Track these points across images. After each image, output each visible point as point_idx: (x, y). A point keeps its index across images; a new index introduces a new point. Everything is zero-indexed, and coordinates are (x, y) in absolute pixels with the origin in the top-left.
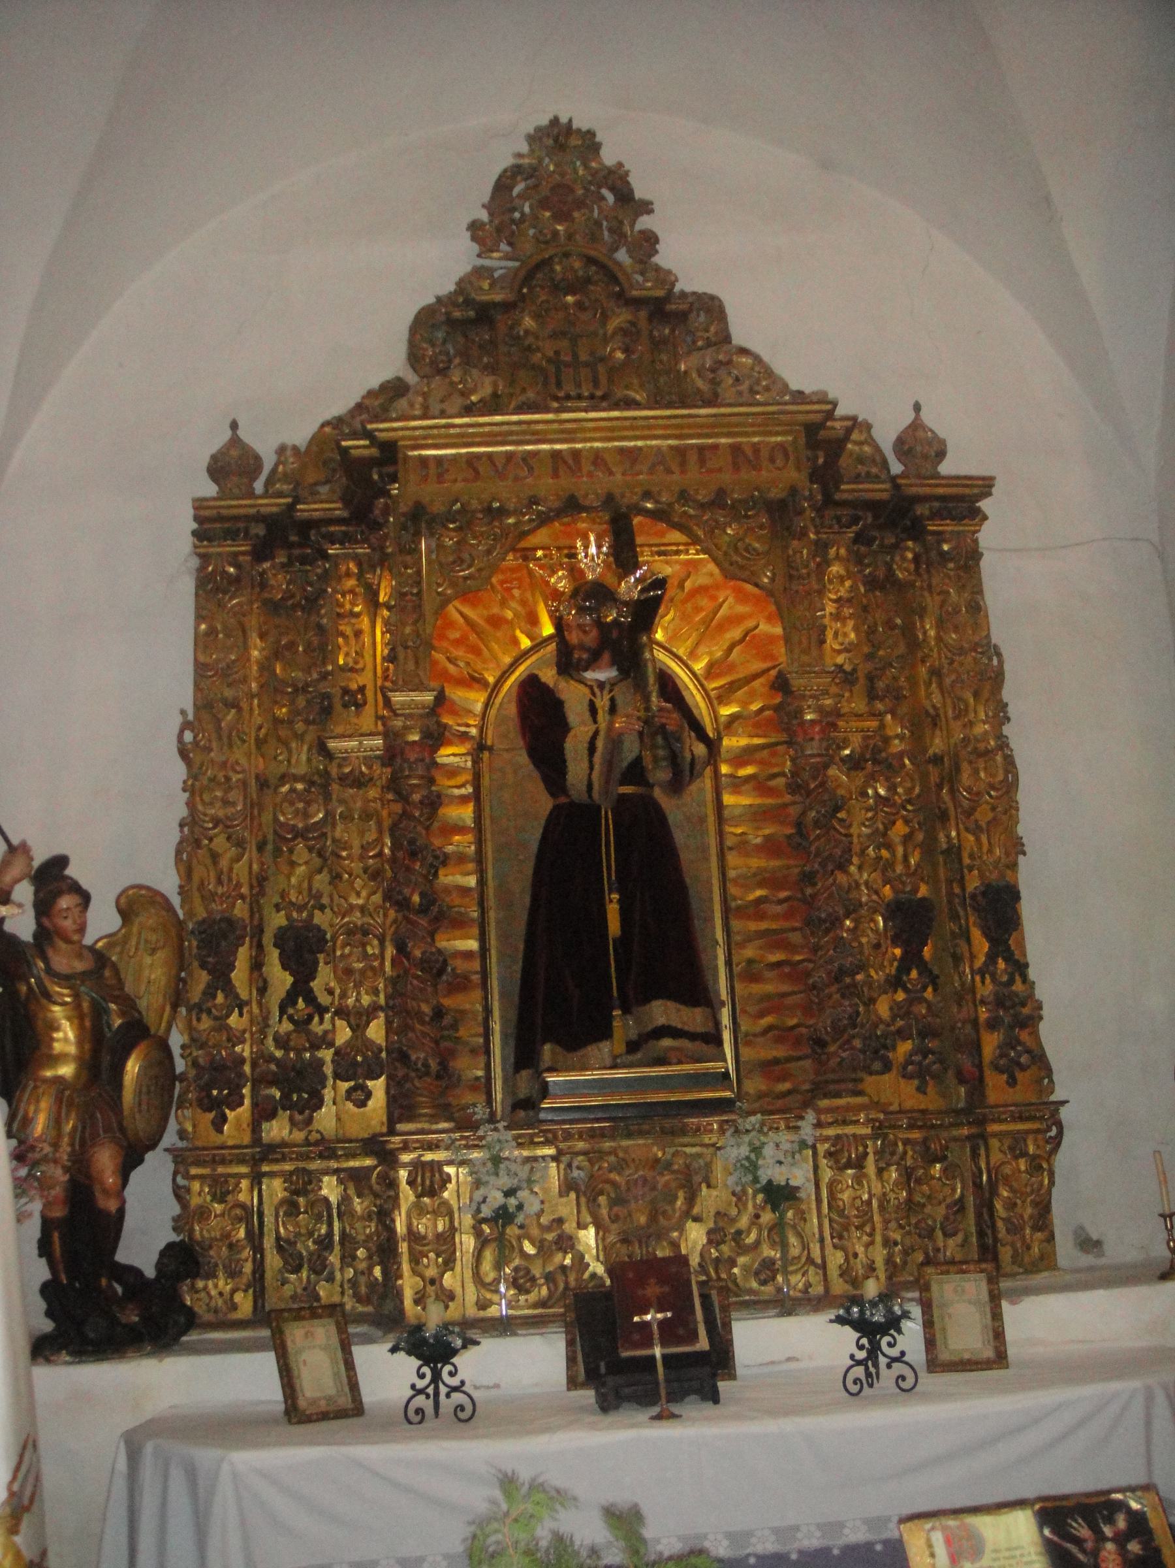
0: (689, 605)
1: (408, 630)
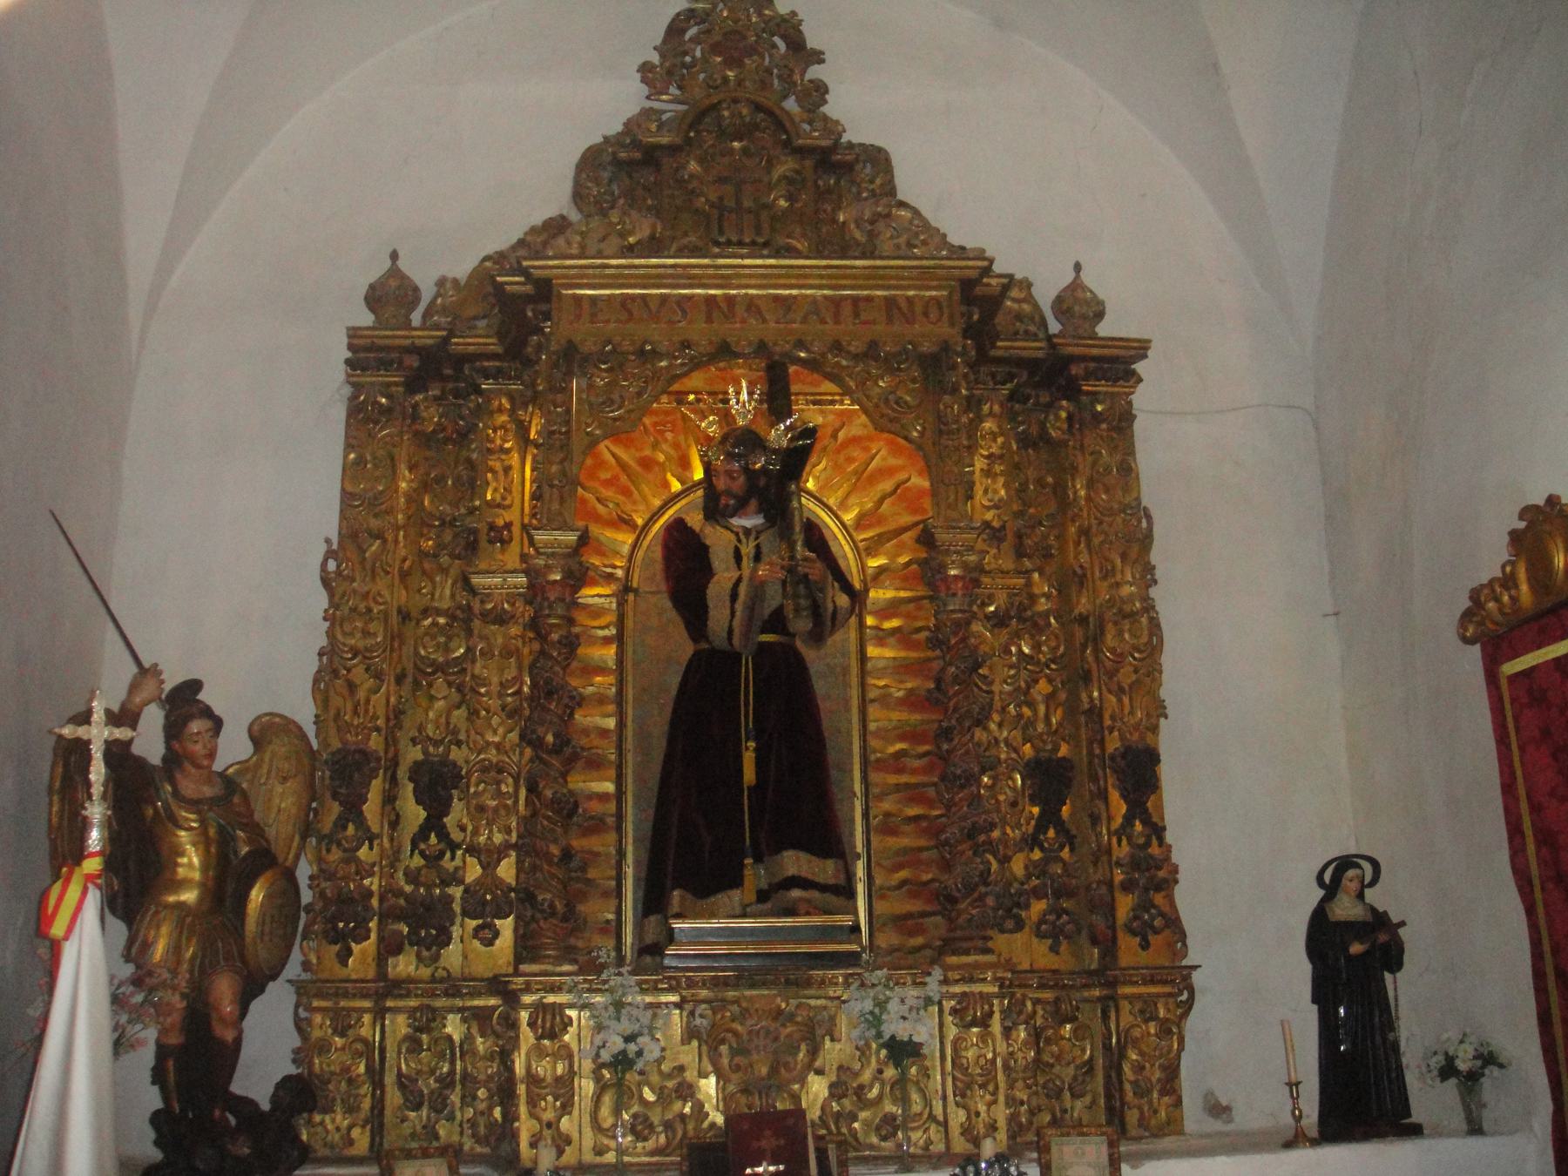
0: (842, 457)
1: (554, 469)
